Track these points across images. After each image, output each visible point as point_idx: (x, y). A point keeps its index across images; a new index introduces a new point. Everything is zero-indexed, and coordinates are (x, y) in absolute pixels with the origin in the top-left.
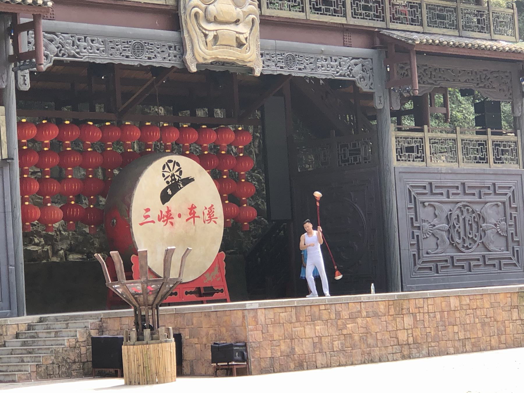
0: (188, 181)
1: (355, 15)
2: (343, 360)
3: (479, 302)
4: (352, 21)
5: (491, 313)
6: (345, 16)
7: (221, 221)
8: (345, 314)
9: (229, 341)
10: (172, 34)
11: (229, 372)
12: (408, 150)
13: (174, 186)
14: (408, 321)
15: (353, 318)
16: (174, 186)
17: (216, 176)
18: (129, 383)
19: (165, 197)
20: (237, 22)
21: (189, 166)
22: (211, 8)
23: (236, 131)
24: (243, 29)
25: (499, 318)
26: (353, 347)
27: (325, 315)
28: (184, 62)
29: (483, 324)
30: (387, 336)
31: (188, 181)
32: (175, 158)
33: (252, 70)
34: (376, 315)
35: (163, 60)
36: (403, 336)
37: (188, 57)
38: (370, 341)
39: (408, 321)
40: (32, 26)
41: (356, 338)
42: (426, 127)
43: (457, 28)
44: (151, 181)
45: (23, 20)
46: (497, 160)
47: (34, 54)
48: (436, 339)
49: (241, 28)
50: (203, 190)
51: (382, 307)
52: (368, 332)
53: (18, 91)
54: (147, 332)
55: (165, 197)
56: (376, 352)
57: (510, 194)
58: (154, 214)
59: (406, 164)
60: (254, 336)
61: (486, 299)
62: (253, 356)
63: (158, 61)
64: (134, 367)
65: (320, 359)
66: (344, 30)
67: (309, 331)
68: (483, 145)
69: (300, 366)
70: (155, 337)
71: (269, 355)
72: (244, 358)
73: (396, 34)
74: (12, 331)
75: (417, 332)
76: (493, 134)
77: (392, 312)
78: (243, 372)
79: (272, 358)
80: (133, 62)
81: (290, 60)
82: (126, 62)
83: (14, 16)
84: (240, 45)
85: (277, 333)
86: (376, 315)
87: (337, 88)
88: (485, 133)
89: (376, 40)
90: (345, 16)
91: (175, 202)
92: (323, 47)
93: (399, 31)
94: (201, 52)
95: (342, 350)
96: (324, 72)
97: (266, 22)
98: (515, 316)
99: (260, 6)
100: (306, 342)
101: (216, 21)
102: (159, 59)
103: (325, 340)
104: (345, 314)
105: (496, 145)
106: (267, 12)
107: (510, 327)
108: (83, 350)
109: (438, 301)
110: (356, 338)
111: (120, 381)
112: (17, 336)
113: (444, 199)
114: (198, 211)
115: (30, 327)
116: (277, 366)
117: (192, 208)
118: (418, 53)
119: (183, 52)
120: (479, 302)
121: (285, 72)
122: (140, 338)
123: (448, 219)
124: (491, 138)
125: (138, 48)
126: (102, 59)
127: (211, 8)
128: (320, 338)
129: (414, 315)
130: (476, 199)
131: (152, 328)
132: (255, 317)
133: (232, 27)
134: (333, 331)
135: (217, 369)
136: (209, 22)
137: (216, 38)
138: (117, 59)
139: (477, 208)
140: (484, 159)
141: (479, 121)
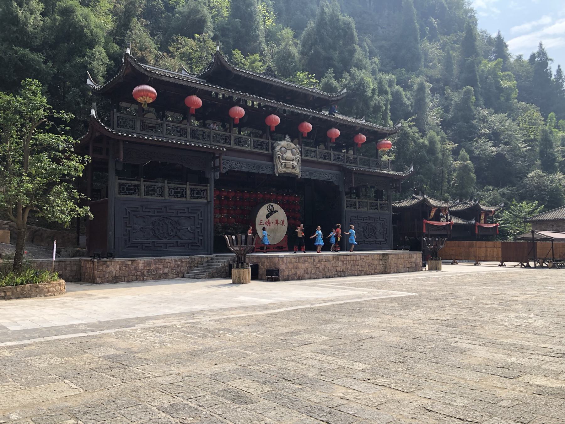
0: (276, 211)
1: (334, 160)
2: (315, 277)
3: (367, 258)
4: (333, 162)
5: (372, 262)
6: (230, 144)
7: (287, 225)
8: (317, 260)
9: (273, 268)
10: (271, 163)
11: (272, 280)
12: (350, 205)
13: (271, 213)
14: (341, 263)
15: (320, 262)
16: (271, 213)
17: (287, 212)
18: (234, 283)
19: (268, 217)
20: (293, 160)
21: (276, 207)
22: (284, 155)
23: (295, 197)
24: (295, 163)
25: (375, 263)
26: (320, 272)
27: (309, 260)
28: (274, 173)
29: (369, 265)
30: (332, 268)
31: (276, 211)
32: (271, 204)
33: (298, 176)
34: (329, 261)
35: (267, 171)
36: (338, 269)
37: (275, 171)
38: (326, 270)
39: (341, 263)
40: (219, 157)
41: (321, 269)
42: (208, 185)
43: (369, 166)
44: (263, 211)
45: (217, 155)
46: (381, 209)
47: (219, 167)
48: (351, 270)
49: (294, 162)
50: (281, 215)
51: (331, 258)
52: (325, 267)
53: (215, 179)
54: (240, 265)
55: (268, 217)
56: (328, 274)
57: (199, 213)
58: (264, 222)
59: (349, 209)
60: (282, 267)
61: (370, 256)
62: (281, 274)
63: (265, 172)
64: (235, 276)
65: (307, 276)
66: (330, 165)
67: (303, 266)
68: (376, 204)
69: (299, 278)
70: (243, 267)
71: (287, 274)
72: (278, 275)
73: (347, 167)
74: (205, 260)
75: (344, 268)
76: (190, 185)
77: (335, 260)
78: (277, 280)
79: (288, 275)
80: (256, 171)
81: (311, 174)
82: (254, 171)
83: (214, 154)
84: (294, 168)
85: (291, 266)
86: (329, 261)
87: (329, 183)
88: (140, 181)
89: (342, 169)
90: (230, 144)
91: (270, 219)
92: (322, 170)
93: (348, 166)
94: (280, 169)
95: (315, 273)
96: (322, 178)
97: (303, 161)
98: (381, 263)
99: (301, 156)
100: (301, 270)
101: (286, 159)
102: (265, 171)
103: (309, 269)
104: (317, 260)
105: (381, 204)
106: (304, 158)
107: (379, 267)
108: (227, 268)
109: (352, 256)
110: (321, 269)
111: (230, 281)
112: (207, 262)
113: (362, 221)
114: (279, 222)
115: (212, 259)
116: (290, 278)
117: (277, 220)
118: (355, 173)
119: (274, 169)
120: (367, 258)
121: (309, 177)
122: (237, 267)
123: (363, 228)
124: (379, 202)
125: (258, 167)
126: (246, 170)
127: (284, 155)
128: (307, 268)
129: (343, 262)
130: (373, 222)
131: (242, 263)
132: (283, 260)
133: (291, 162)
134: (312, 266)
135: (268, 278)
136: (283, 160)
137: (285, 165)
138: (251, 170)
139: (374, 224)
140: (377, 209)
141: (375, 197)
